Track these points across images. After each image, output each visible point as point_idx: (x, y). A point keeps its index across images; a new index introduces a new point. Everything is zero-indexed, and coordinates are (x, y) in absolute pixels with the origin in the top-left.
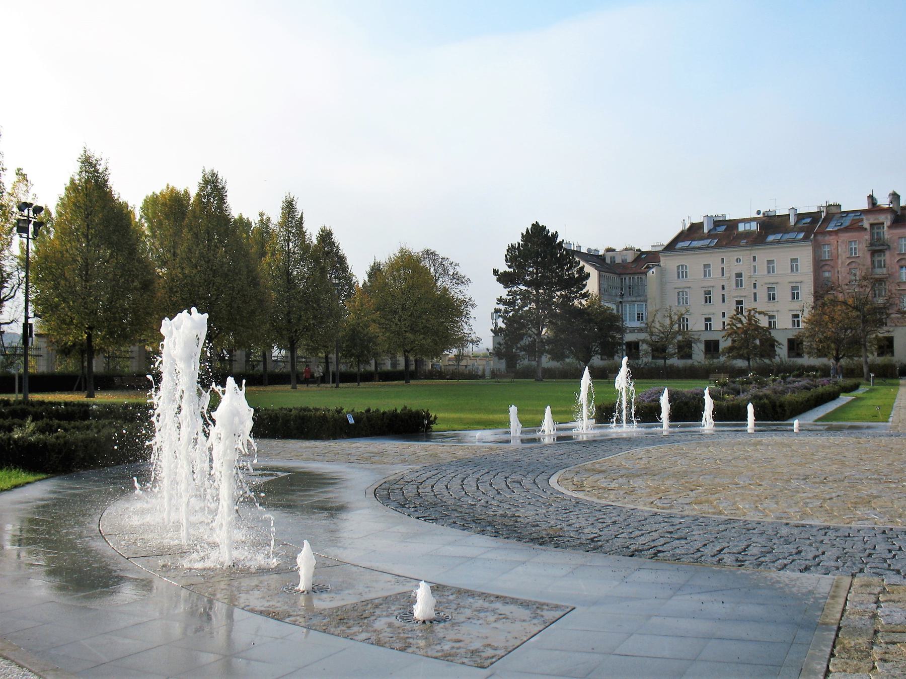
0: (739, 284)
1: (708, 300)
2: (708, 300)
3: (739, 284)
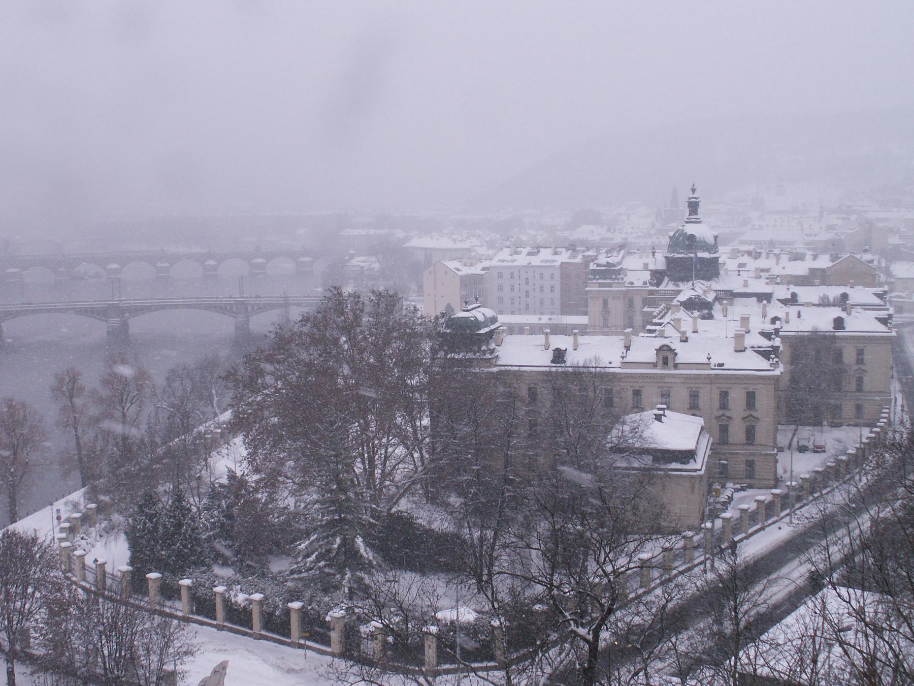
0: (527, 283)
1: (512, 290)
2: (512, 290)
3: (527, 283)
